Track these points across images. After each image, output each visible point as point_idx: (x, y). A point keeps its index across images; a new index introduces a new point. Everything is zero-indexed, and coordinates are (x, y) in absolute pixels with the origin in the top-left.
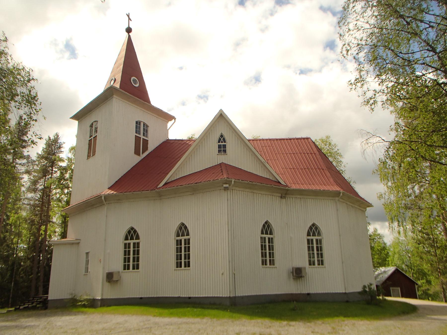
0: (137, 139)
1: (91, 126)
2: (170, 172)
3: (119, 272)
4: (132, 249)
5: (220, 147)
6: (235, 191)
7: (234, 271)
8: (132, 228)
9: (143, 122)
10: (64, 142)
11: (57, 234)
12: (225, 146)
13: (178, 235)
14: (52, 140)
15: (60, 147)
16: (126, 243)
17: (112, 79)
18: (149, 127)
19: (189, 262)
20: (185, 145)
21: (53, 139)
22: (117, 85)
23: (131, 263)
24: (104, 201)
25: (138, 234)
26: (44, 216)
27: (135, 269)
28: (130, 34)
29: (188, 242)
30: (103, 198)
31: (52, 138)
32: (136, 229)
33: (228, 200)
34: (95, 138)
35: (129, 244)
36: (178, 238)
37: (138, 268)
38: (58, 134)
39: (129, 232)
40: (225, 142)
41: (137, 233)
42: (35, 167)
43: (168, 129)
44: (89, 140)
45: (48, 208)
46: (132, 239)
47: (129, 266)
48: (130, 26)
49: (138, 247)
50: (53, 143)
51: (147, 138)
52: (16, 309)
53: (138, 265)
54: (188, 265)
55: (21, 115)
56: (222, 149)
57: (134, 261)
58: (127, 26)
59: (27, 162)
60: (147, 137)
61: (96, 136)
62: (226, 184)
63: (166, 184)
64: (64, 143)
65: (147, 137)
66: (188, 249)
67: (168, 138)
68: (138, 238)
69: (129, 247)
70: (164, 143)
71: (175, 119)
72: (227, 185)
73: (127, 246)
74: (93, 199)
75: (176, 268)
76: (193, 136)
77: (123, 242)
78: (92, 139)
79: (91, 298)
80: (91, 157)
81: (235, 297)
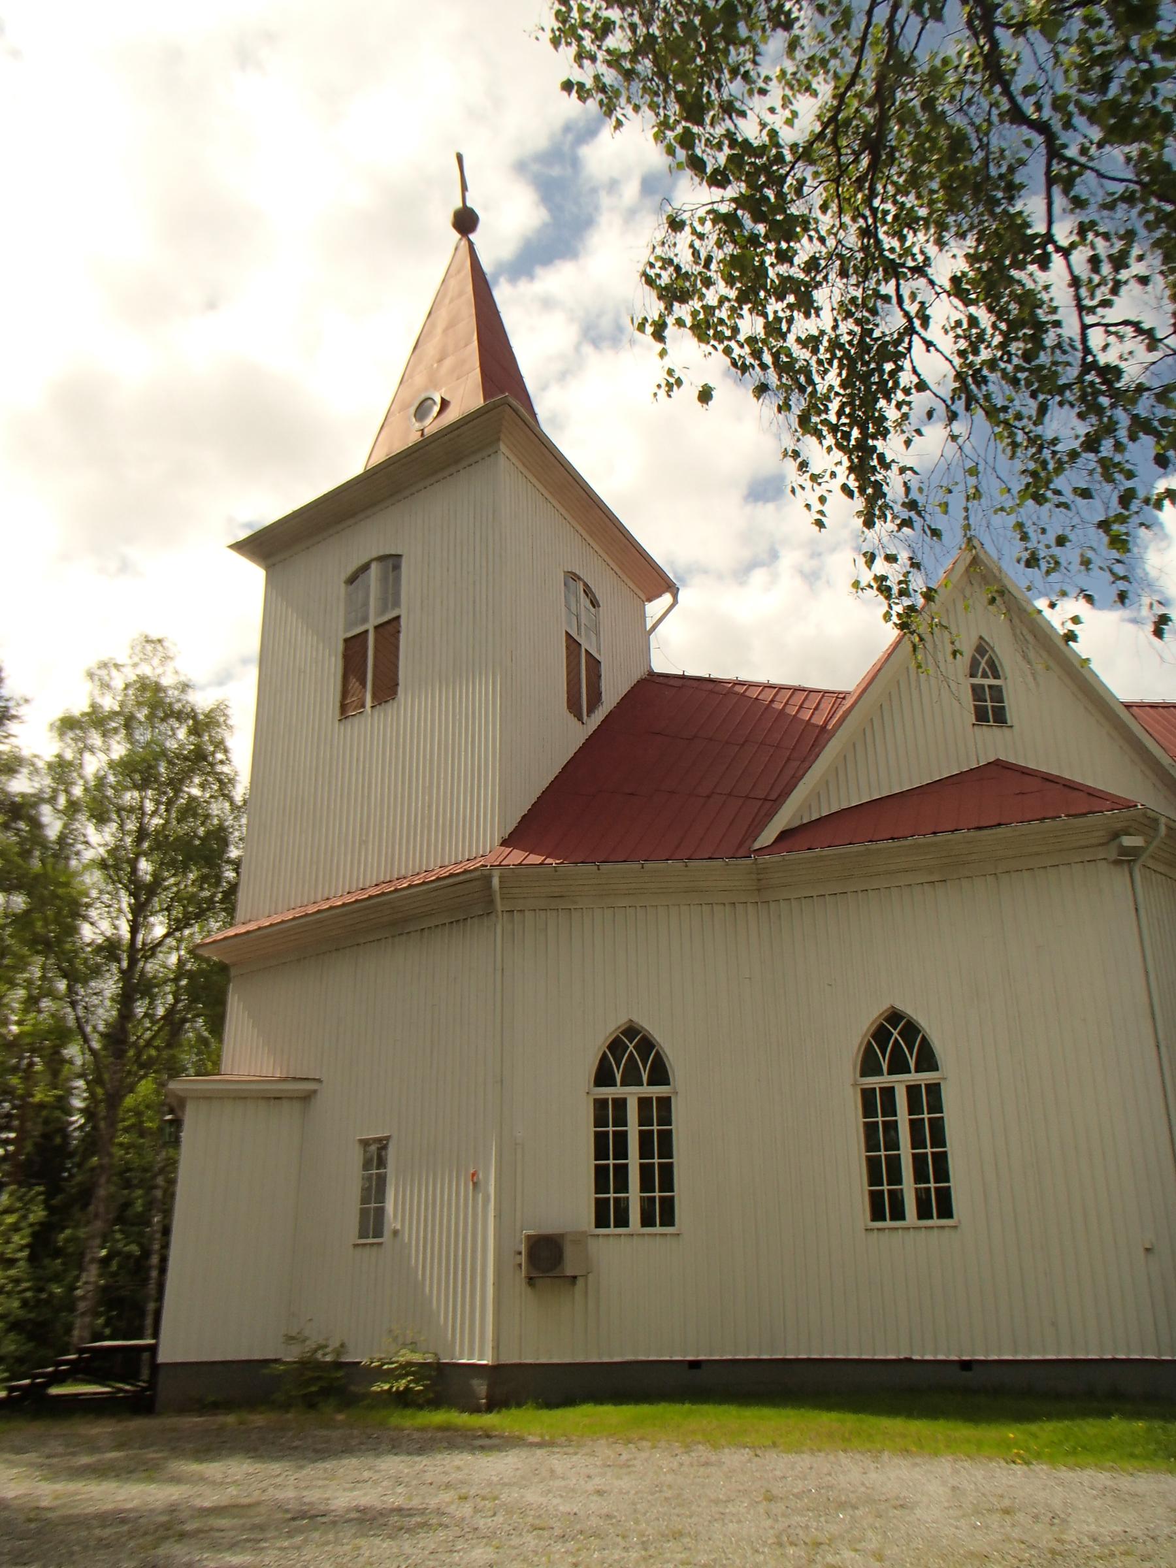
4: (633, 1130)
8: (894, 1017)
12: (997, 693)
16: (605, 1101)
23: (908, 1187)
27: (653, 1225)
28: (472, 237)
34: (389, 628)
37: (668, 1218)
39: (880, 1035)
41: (924, 1039)
43: (649, 627)
44: (346, 641)
46: (633, 1078)
48: (469, 204)
49: (936, 1105)
53: (668, 1207)
55: (947, 248)
58: (459, 204)
63: (784, 835)
68: (660, 1075)
69: (621, 1120)
70: (641, 683)
71: (675, 593)
77: (855, 1085)
79: (430, 1359)
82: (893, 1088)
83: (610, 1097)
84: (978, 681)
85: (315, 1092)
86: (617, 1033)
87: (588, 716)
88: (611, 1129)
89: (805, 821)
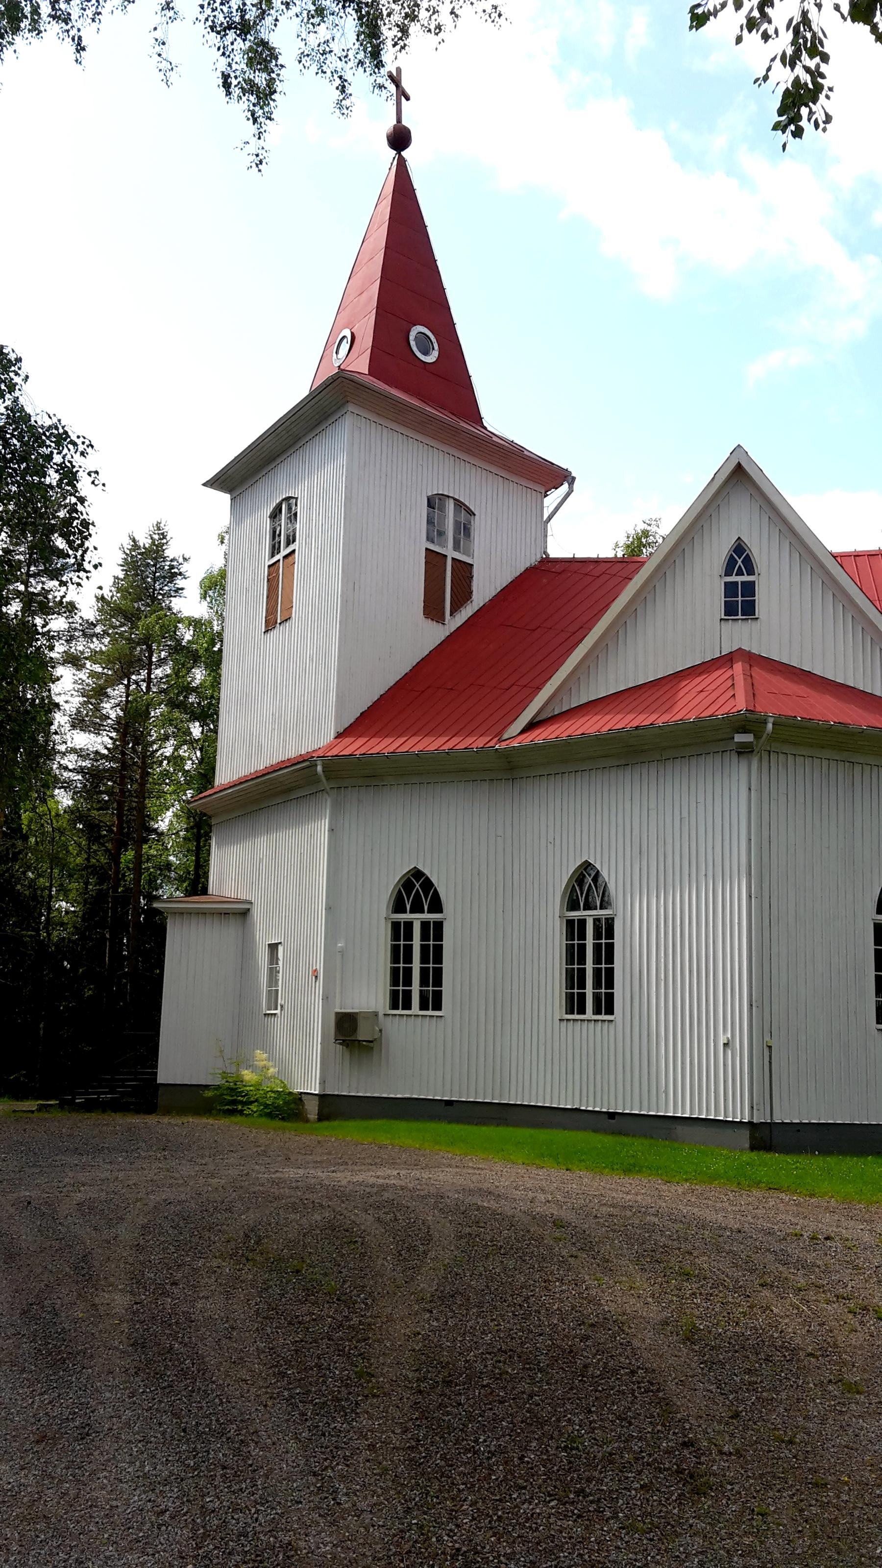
0: (434, 560)
1: (275, 515)
2: (548, 685)
3: (376, 1014)
5: (731, 589)
6: (781, 756)
7: (767, 1038)
8: (417, 874)
9: (455, 499)
10: (187, 556)
11: (173, 875)
12: (749, 589)
13: (573, 905)
14: (144, 550)
15: (172, 575)
17: (344, 337)
18: (477, 517)
19: (610, 998)
20: (605, 578)
21: (147, 546)
22: (361, 365)
24: (323, 779)
25: (436, 893)
26: (131, 809)
27: (600, 1013)
29: (606, 928)
30: (319, 768)
31: (144, 541)
32: (429, 876)
33: (750, 789)
34: (290, 558)
35: (409, 925)
36: (575, 914)
37: (438, 1006)
38: (162, 525)
40: (751, 572)
41: (436, 891)
42: (96, 645)
43: (546, 516)
44: (269, 566)
45: (143, 784)
46: (417, 908)
47: (408, 995)
48: (405, 122)
49: (439, 936)
50: (149, 561)
51: (469, 556)
52: (61, 1106)
53: (438, 996)
54: (605, 1005)
56: (740, 599)
57: (424, 982)
59: (66, 626)
60: (467, 553)
61: (294, 551)
62: (745, 731)
64: (185, 559)
65: (467, 553)
66: (605, 953)
67: (545, 553)
68: (436, 906)
69: (409, 936)
71: (572, 481)
72: (748, 738)
73: (401, 931)
74: (285, 771)
75: (593, 1014)
76: (653, 529)
78: (279, 561)
80: (278, 625)
81: (771, 1125)
82: (585, 920)
83: (402, 921)
84: (733, 578)
85: (249, 910)
86: (409, 875)
87: (452, 614)
88: (402, 943)
89: (556, 713)
